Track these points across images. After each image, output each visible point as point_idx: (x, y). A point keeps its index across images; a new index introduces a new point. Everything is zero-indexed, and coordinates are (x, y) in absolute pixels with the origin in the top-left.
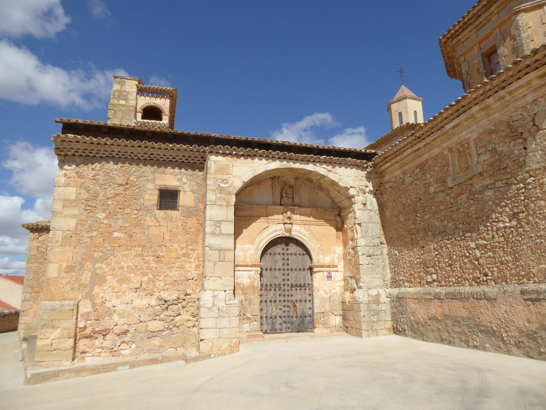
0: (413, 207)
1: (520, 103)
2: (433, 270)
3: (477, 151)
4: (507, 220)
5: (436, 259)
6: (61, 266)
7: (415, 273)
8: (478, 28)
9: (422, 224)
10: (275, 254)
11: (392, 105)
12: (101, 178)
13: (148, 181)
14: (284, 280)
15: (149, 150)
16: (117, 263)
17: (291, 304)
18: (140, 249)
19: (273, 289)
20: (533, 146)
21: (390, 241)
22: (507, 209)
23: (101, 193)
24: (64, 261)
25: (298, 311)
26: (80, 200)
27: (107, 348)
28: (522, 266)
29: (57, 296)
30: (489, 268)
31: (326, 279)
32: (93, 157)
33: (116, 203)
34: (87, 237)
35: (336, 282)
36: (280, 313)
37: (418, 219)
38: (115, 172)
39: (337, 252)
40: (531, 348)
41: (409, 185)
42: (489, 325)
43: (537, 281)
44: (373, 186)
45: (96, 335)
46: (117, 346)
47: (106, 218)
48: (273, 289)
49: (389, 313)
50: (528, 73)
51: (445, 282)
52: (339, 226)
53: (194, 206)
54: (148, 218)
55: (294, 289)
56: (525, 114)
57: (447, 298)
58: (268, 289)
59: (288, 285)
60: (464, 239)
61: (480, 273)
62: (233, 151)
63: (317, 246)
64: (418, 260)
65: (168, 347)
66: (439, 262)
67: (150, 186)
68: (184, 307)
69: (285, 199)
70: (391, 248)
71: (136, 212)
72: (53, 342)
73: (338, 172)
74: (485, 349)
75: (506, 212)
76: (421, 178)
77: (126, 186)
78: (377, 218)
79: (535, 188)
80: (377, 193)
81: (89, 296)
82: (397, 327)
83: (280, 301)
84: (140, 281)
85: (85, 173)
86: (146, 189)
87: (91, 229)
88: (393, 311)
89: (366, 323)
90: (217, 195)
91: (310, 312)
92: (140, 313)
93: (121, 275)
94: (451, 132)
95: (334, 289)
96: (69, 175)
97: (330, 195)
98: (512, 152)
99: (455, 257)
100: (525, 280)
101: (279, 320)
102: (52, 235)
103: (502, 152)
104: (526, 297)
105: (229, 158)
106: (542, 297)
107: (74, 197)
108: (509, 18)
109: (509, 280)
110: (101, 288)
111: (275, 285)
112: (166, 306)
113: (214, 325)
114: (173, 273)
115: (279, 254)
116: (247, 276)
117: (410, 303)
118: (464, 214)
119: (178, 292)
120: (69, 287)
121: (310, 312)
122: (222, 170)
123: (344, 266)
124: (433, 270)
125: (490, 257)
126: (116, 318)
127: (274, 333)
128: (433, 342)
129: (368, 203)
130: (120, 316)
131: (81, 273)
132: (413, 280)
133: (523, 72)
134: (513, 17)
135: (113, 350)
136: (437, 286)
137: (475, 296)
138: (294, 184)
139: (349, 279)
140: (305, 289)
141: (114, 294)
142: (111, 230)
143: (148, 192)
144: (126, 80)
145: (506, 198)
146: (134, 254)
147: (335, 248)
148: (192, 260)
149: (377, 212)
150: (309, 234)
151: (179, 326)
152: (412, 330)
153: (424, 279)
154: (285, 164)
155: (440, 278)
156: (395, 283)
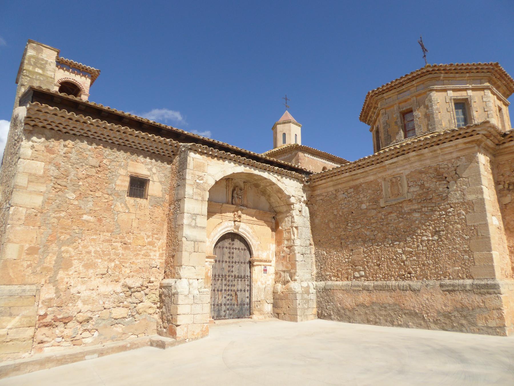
0: (345, 218)
1: (447, 157)
2: (361, 268)
3: (408, 184)
4: (430, 235)
6: (22, 247)
7: (343, 270)
8: (399, 93)
9: (352, 232)
11: (278, 126)
12: (73, 156)
13: (120, 166)
15: (126, 136)
16: (84, 247)
17: (233, 294)
18: (109, 234)
19: (220, 279)
20: (455, 187)
22: (431, 228)
23: (73, 173)
24: (26, 242)
25: (238, 299)
26: (48, 176)
27: (68, 337)
28: (441, 268)
29: (16, 280)
30: (413, 268)
32: (66, 133)
33: (87, 185)
34: (54, 217)
36: (224, 301)
37: (349, 228)
38: (88, 153)
39: (272, 249)
40: (446, 324)
41: (341, 200)
42: (412, 309)
43: (452, 278)
45: (56, 323)
47: (76, 199)
48: (220, 279)
49: (315, 301)
50: (457, 139)
51: (372, 277)
52: (274, 227)
53: (161, 196)
54: (118, 204)
56: (450, 165)
57: (375, 289)
58: (217, 279)
59: (232, 276)
60: (392, 246)
61: (405, 272)
62: (210, 151)
64: (346, 260)
65: (130, 334)
67: (122, 172)
68: (146, 294)
69: (236, 199)
70: (319, 249)
71: (107, 196)
72: (10, 332)
74: (408, 326)
75: (430, 230)
76: (354, 197)
78: (308, 224)
79: (454, 216)
80: (309, 203)
81: (53, 281)
84: (106, 266)
85: (55, 148)
86: (118, 175)
87: (59, 209)
88: (319, 300)
90: (194, 190)
94: (387, 166)
96: (37, 148)
97: (270, 200)
98: (437, 189)
99: (383, 259)
100: (442, 277)
102: (14, 212)
103: (429, 188)
104: (444, 289)
105: (205, 157)
106: (456, 289)
107: (41, 173)
108: (425, 93)
109: (429, 277)
110: (66, 272)
111: (222, 276)
112: (130, 293)
115: (226, 248)
117: (338, 294)
118: (393, 228)
120: (30, 270)
123: (276, 262)
125: (414, 260)
126: (80, 304)
127: (220, 319)
128: (359, 323)
129: (303, 211)
130: (85, 302)
131: (45, 255)
132: (340, 275)
133: (455, 138)
134: (428, 93)
135: (75, 338)
137: (402, 288)
139: (282, 274)
140: (245, 280)
141: (80, 279)
143: (120, 178)
144: (44, 48)
145: (430, 220)
146: (102, 239)
148: (157, 249)
151: (141, 313)
152: (338, 315)
155: (368, 275)
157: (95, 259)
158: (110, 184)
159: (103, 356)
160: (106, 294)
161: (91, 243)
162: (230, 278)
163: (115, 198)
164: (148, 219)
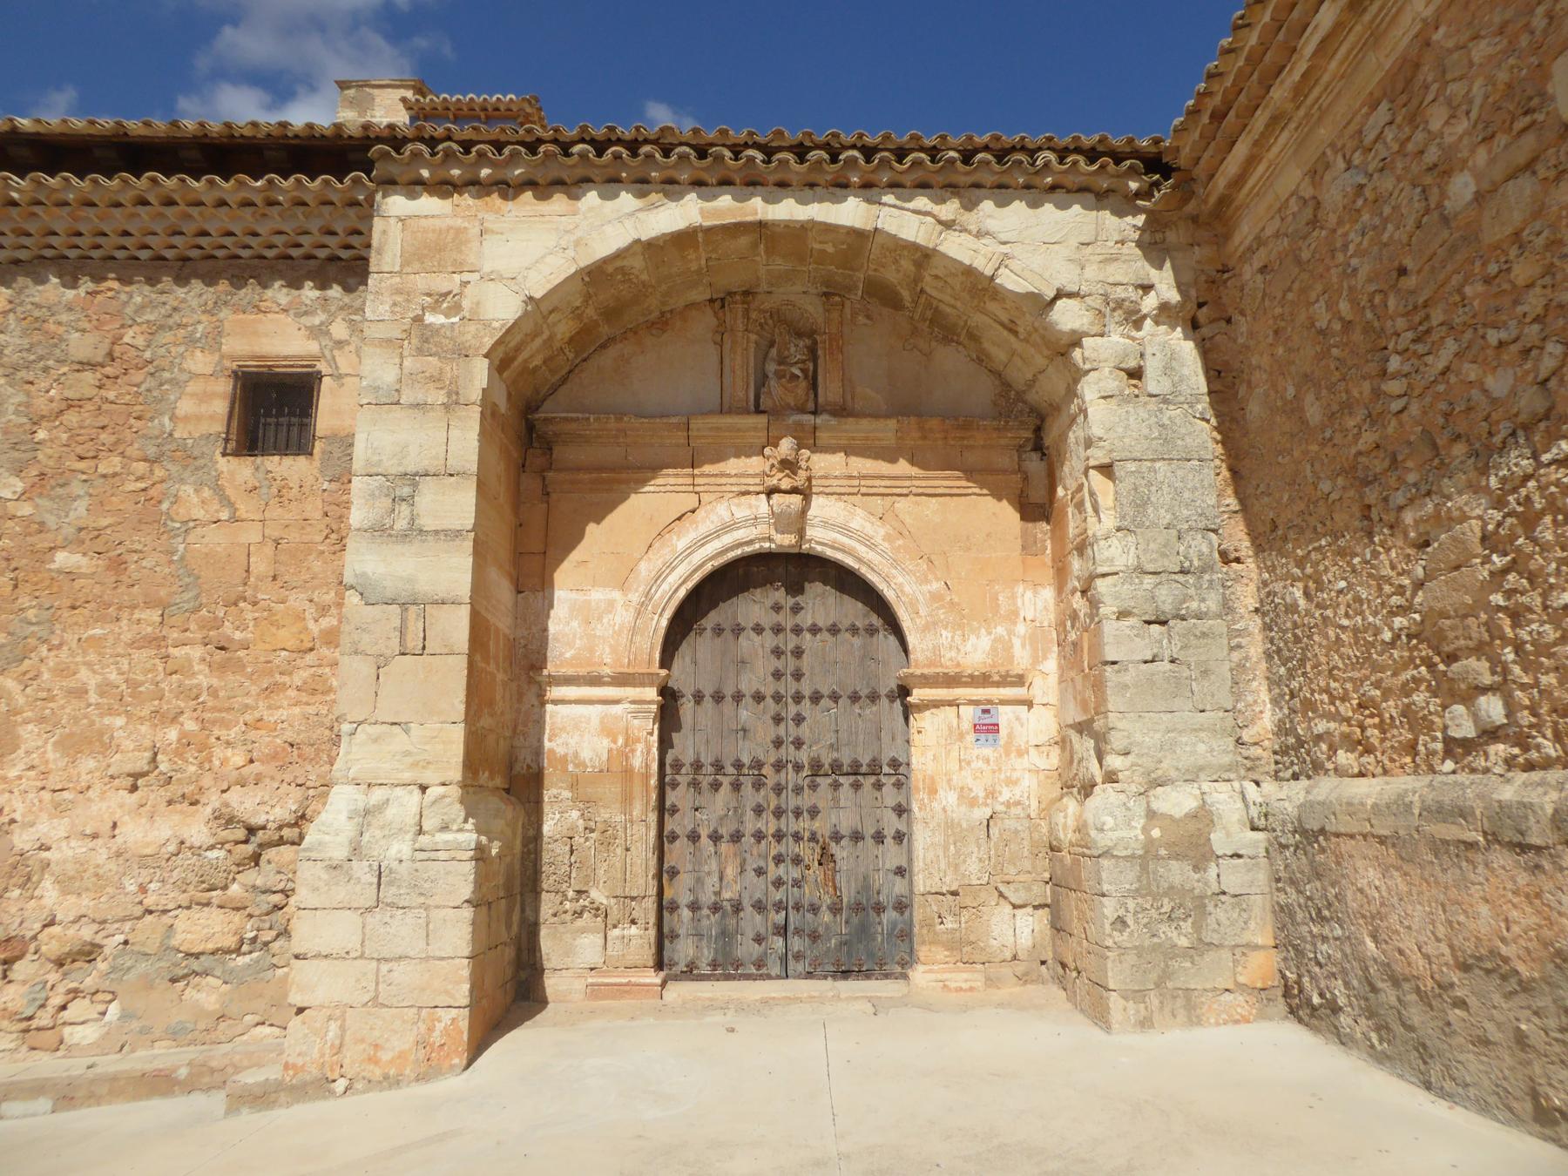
0: (1368, 329)
2: (1478, 669)
5: (1497, 599)
9: (1415, 409)
10: (738, 630)
13: (191, 341)
14: (778, 743)
16: (64, 671)
17: (808, 852)
19: (726, 781)
21: (1267, 537)
25: (841, 879)
31: (971, 737)
35: (1021, 753)
36: (758, 888)
38: (64, 317)
44: (1180, 286)
46: (50, 1010)
48: (726, 781)
49: (1260, 905)
54: (187, 490)
55: (824, 782)
58: (705, 782)
59: (798, 768)
63: (926, 588)
64: (1399, 622)
66: (1517, 616)
67: (200, 362)
71: (141, 467)
73: (991, 224)
77: (108, 370)
78: (1202, 435)
80: (1203, 314)
82: (1299, 983)
83: (759, 836)
84: (147, 743)
88: (1282, 898)
89: (1131, 958)
90: (406, 363)
91: (899, 886)
92: (144, 876)
93: (76, 720)
95: (1011, 782)
101: (752, 921)
105: (466, 200)
112: (250, 848)
113: (353, 943)
114: (283, 714)
115: (758, 629)
116: (595, 722)
117: (1360, 864)
119: (297, 793)
121: (899, 886)
122: (433, 251)
124: (1478, 669)
126: (49, 892)
127: (728, 977)
128: (1483, 1108)
129: (1152, 368)
130: (67, 885)
132: (1374, 734)
136: (1510, 763)
138: (820, 320)
139: (1074, 736)
140: (878, 786)
142: (42, 542)
143: (192, 387)
144: (376, 92)
146: (127, 637)
147: (1013, 597)
149: (1203, 405)
150: (887, 538)
152: (1371, 1014)
153: (1430, 727)
154: (725, 207)
156: (1297, 755)
157: (102, 715)
158: (152, 419)
159: (74, 1108)
160: (148, 851)
161: (85, 653)
162: (789, 777)
163: (174, 468)
164: (319, 538)
